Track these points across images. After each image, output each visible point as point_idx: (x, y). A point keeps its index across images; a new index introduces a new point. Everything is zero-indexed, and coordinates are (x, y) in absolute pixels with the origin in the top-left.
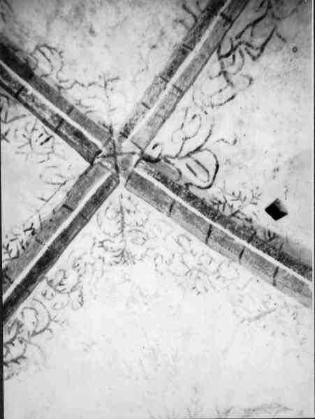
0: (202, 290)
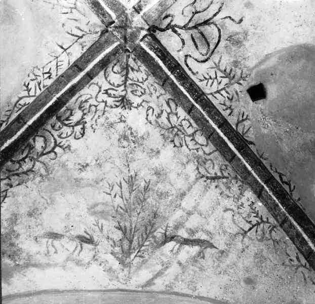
0: (178, 144)
